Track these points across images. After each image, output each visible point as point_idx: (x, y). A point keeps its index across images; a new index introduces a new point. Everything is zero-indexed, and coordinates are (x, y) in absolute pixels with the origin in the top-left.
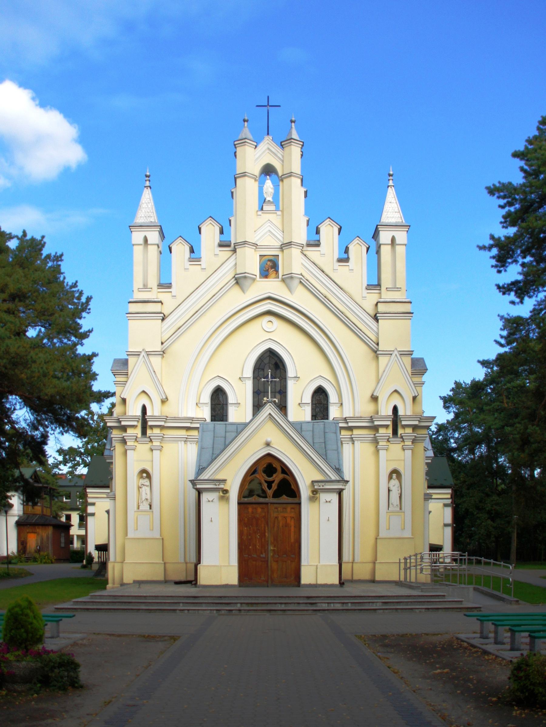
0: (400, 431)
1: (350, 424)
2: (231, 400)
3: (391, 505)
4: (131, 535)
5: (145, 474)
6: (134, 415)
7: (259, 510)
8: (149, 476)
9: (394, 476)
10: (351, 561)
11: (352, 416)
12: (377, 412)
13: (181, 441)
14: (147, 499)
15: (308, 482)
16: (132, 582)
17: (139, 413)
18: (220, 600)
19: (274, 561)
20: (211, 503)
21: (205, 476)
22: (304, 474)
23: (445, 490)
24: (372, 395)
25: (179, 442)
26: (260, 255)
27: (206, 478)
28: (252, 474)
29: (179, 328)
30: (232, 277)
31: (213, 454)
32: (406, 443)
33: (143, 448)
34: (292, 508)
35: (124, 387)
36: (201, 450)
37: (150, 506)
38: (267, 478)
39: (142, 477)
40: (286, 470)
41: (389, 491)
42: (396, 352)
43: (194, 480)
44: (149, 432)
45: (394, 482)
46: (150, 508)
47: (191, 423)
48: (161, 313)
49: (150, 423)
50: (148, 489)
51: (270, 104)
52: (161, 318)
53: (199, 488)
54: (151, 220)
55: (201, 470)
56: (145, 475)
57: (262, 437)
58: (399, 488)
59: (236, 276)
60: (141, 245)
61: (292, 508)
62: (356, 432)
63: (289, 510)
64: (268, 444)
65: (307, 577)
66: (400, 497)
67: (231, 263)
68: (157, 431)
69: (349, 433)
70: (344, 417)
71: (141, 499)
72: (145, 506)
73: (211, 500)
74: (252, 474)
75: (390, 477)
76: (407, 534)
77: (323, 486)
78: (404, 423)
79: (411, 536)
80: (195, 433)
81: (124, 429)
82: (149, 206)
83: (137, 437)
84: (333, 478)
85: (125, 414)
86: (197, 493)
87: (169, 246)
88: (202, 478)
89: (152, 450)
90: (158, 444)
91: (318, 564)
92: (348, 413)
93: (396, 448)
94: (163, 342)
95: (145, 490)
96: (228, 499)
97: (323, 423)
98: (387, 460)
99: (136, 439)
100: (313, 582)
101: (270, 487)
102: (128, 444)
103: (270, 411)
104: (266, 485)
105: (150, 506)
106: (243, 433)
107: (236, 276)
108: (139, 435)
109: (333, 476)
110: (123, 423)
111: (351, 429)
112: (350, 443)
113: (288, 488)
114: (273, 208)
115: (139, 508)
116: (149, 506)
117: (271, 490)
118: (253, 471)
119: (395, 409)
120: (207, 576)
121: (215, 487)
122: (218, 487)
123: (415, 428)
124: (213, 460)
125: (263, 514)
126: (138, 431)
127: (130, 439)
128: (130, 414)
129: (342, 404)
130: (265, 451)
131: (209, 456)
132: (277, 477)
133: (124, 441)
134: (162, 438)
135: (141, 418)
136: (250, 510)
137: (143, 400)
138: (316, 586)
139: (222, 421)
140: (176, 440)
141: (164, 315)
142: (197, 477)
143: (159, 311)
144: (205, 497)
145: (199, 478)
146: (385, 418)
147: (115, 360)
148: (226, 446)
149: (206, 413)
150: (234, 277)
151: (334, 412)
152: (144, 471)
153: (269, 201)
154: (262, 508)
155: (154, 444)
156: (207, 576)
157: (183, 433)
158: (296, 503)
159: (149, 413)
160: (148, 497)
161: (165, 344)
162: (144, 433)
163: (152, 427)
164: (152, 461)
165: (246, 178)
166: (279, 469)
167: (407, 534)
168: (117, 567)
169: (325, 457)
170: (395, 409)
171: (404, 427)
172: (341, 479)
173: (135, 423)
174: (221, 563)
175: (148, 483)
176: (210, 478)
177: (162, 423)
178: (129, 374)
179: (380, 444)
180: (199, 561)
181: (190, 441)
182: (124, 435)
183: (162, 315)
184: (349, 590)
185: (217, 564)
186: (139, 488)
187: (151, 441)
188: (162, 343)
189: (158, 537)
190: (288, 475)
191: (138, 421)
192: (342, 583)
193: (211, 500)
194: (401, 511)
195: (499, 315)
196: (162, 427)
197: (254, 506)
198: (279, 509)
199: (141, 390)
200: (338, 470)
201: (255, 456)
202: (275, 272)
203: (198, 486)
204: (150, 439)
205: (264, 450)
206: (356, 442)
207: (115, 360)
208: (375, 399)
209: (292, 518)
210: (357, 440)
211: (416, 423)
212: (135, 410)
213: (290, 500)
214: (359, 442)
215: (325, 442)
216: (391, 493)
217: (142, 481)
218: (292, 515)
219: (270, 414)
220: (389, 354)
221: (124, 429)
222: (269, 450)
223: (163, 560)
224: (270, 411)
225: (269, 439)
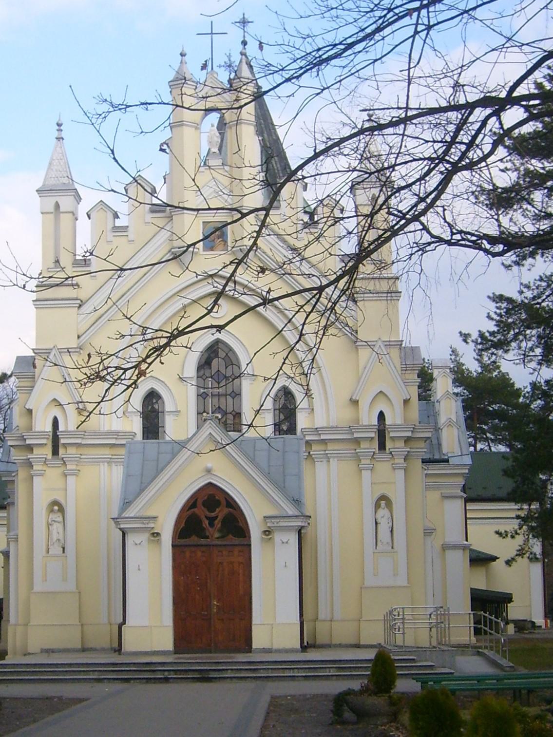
0: (389, 445)
1: (323, 437)
2: (169, 406)
3: (379, 543)
4: (37, 588)
5: (57, 507)
6: (43, 430)
7: (199, 554)
8: (62, 510)
9: (383, 503)
10: (329, 619)
11: (325, 425)
12: (358, 421)
13: (103, 462)
14: (59, 540)
15: (259, 517)
16: (39, 651)
17: (49, 428)
18: (148, 672)
19: (219, 620)
20: (139, 546)
21: (132, 512)
22: (255, 510)
23: (489, 504)
24: (350, 400)
25: (101, 464)
26: (203, 222)
27: (132, 515)
28: (190, 508)
29: (100, 318)
30: (167, 251)
31: (142, 483)
32: (396, 461)
33: (53, 474)
34: (240, 551)
35: (31, 393)
36: (127, 476)
37: (64, 548)
38: (208, 513)
39: (52, 511)
40: (231, 503)
41: (376, 523)
42: (380, 343)
43: (117, 519)
44: (61, 451)
45: (383, 512)
46: (64, 552)
47: (116, 438)
48: (77, 299)
49: (62, 441)
50: (60, 526)
51: (213, 32)
52: (78, 305)
53: (123, 528)
54: (64, 182)
55: (126, 503)
56: (56, 508)
57: (201, 462)
58: (390, 519)
59: (173, 250)
60: (52, 213)
61: (240, 551)
62: (330, 446)
63: (236, 553)
64: (209, 471)
65: (260, 638)
66: (392, 531)
67: (164, 235)
68: (72, 451)
69: (322, 447)
70: (316, 427)
71: (52, 539)
72: (56, 550)
73: (138, 542)
74: (190, 508)
75: (377, 506)
76: (402, 581)
77: (277, 523)
78: (392, 434)
79: (406, 584)
80: (122, 451)
81: (30, 448)
82: (62, 164)
83: (46, 459)
84: (290, 513)
85: (31, 430)
86: (121, 533)
87: (87, 213)
88: (127, 516)
89: (66, 476)
90: (74, 467)
91: (274, 621)
92: (320, 421)
93: (383, 467)
94: (80, 335)
95: (57, 528)
96: (159, 542)
97: (282, 439)
98: (372, 483)
99: (45, 462)
100: (267, 645)
101: (211, 524)
102: (34, 467)
103: (210, 431)
104: (207, 522)
105: (64, 548)
106: (165, 472)
107: (173, 250)
108: (50, 456)
109: (291, 510)
110: (28, 442)
111: (324, 442)
112: (325, 460)
113: (235, 525)
114: (219, 162)
115: (48, 552)
116: (62, 549)
117: (211, 531)
118: (192, 503)
119: (381, 416)
120: (133, 642)
121: (144, 526)
122: (146, 526)
123: (407, 440)
124: (142, 490)
125: (204, 559)
126: (48, 451)
127: (38, 462)
128: (37, 430)
129: (313, 409)
130: (203, 481)
131: (137, 486)
132: (221, 512)
133: (29, 464)
134: (79, 460)
135: (51, 434)
136: (188, 554)
137: (56, 412)
138: (269, 651)
139: (156, 439)
140: (97, 461)
141: (82, 301)
142: (120, 514)
143: (75, 296)
144: (130, 539)
145: (123, 515)
146: (368, 428)
147: (18, 358)
148: (158, 472)
149: (136, 425)
150: (169, 251)
151: (302, 421)
152: (55, 503)
153: (214, 153)
154: (202, 552)
155: (69, 467)
156: (133, 642)
157: (107, 452)
158: (246, 545)
159: (61, 428)
160: (61, 537)
161: (82, 338)
162: (55, 452)
163: (65, 446)
164: (66, 490)
165: (184, 127)
166: (224, 502)
167: (402, 581)
168: (20, 629)
169: (281, 488)
170: (381, 416)
171: (393, 439)
172: (301, 514)
173: (44, 441)
174: (151, 622)
175: (61, 519)
176: (137, 515)
177: (79, 441)
178: (36, 376)
179: (363, 462)
180: (124, 622)
181: (115, 462)
182: (29, 457)
183: (79, 302)
184: (312, 655)
185: (147, 625)
186: (49, 525)
187: (64, 463)
188: (79, 337)
189: (74, 589)
190: (235, 509)
191: (47, 438)
192: (304, 648)
193: (138, 542)
194: (392, 550)
195: (460, 333)
196: (78, 445)
197: (193, 549)
198: (224, 553)
199: (52, 398)
200: (297, 502)
201: (196, 484)
202: (223, 243)
203: (122, 526)
204: (64, 461)
205: (205, 478)
206: (331, 460)
207: (18, 358)
208: (355, 403)
209: (240, 563)
210: (334, 457)
211: (409, 434)
212: (43, 425)
213: (237, 541)
214: (336, 459)
215: (283, 465)
216: (379, 526)
217: (53, 516)
218: (241, 559)
219: (210, 433)
220: (369, 345)
221: (30, 448)
222: (212, 479)
223: (80, 622)
224: (210, 431)
225: (209, 465)
